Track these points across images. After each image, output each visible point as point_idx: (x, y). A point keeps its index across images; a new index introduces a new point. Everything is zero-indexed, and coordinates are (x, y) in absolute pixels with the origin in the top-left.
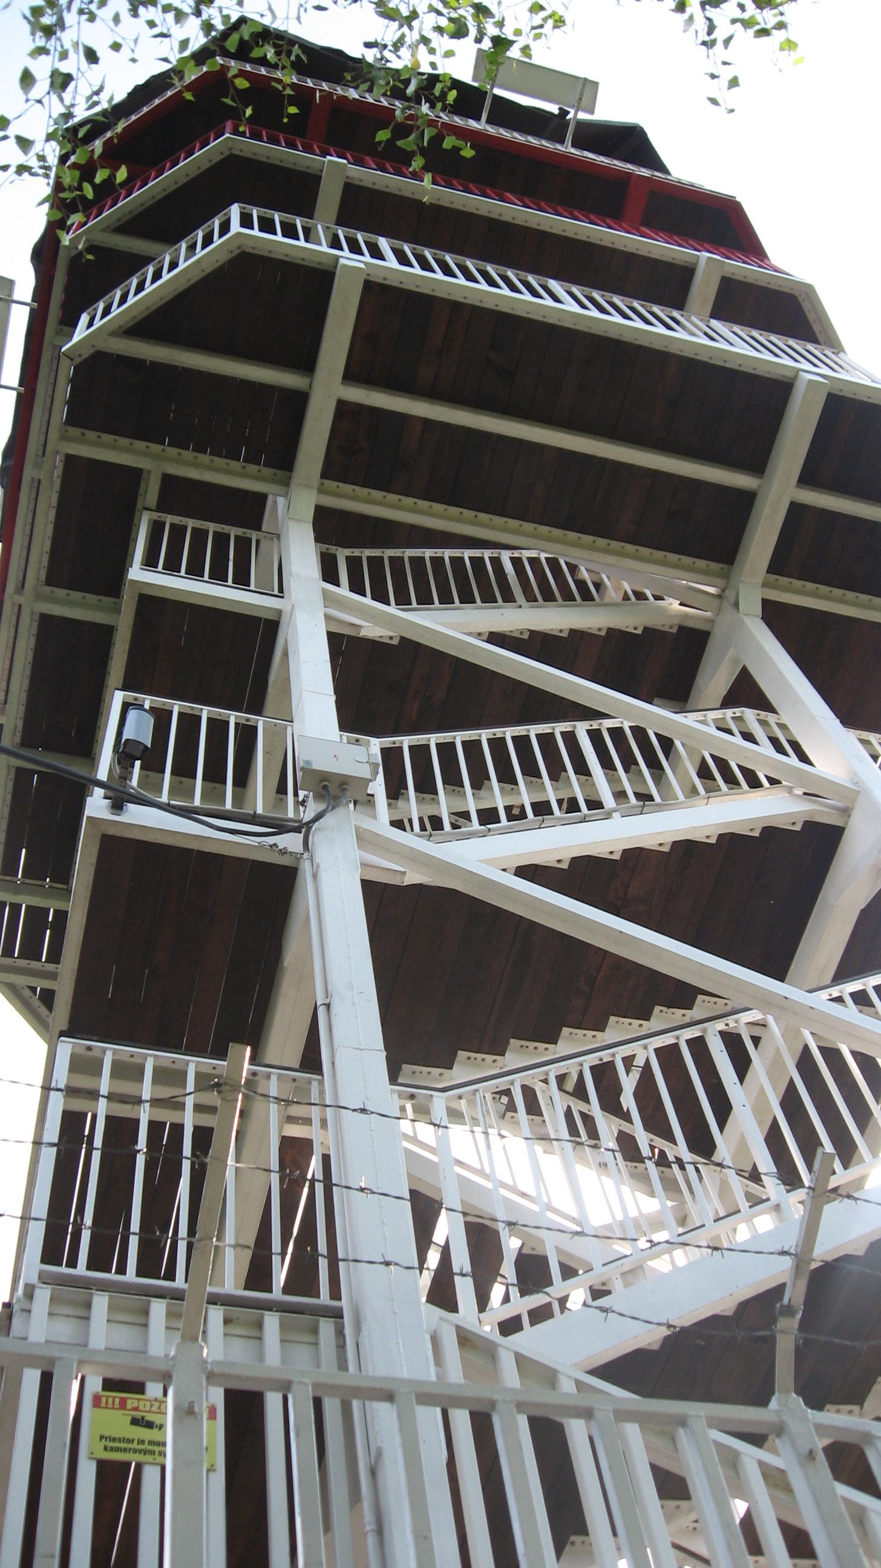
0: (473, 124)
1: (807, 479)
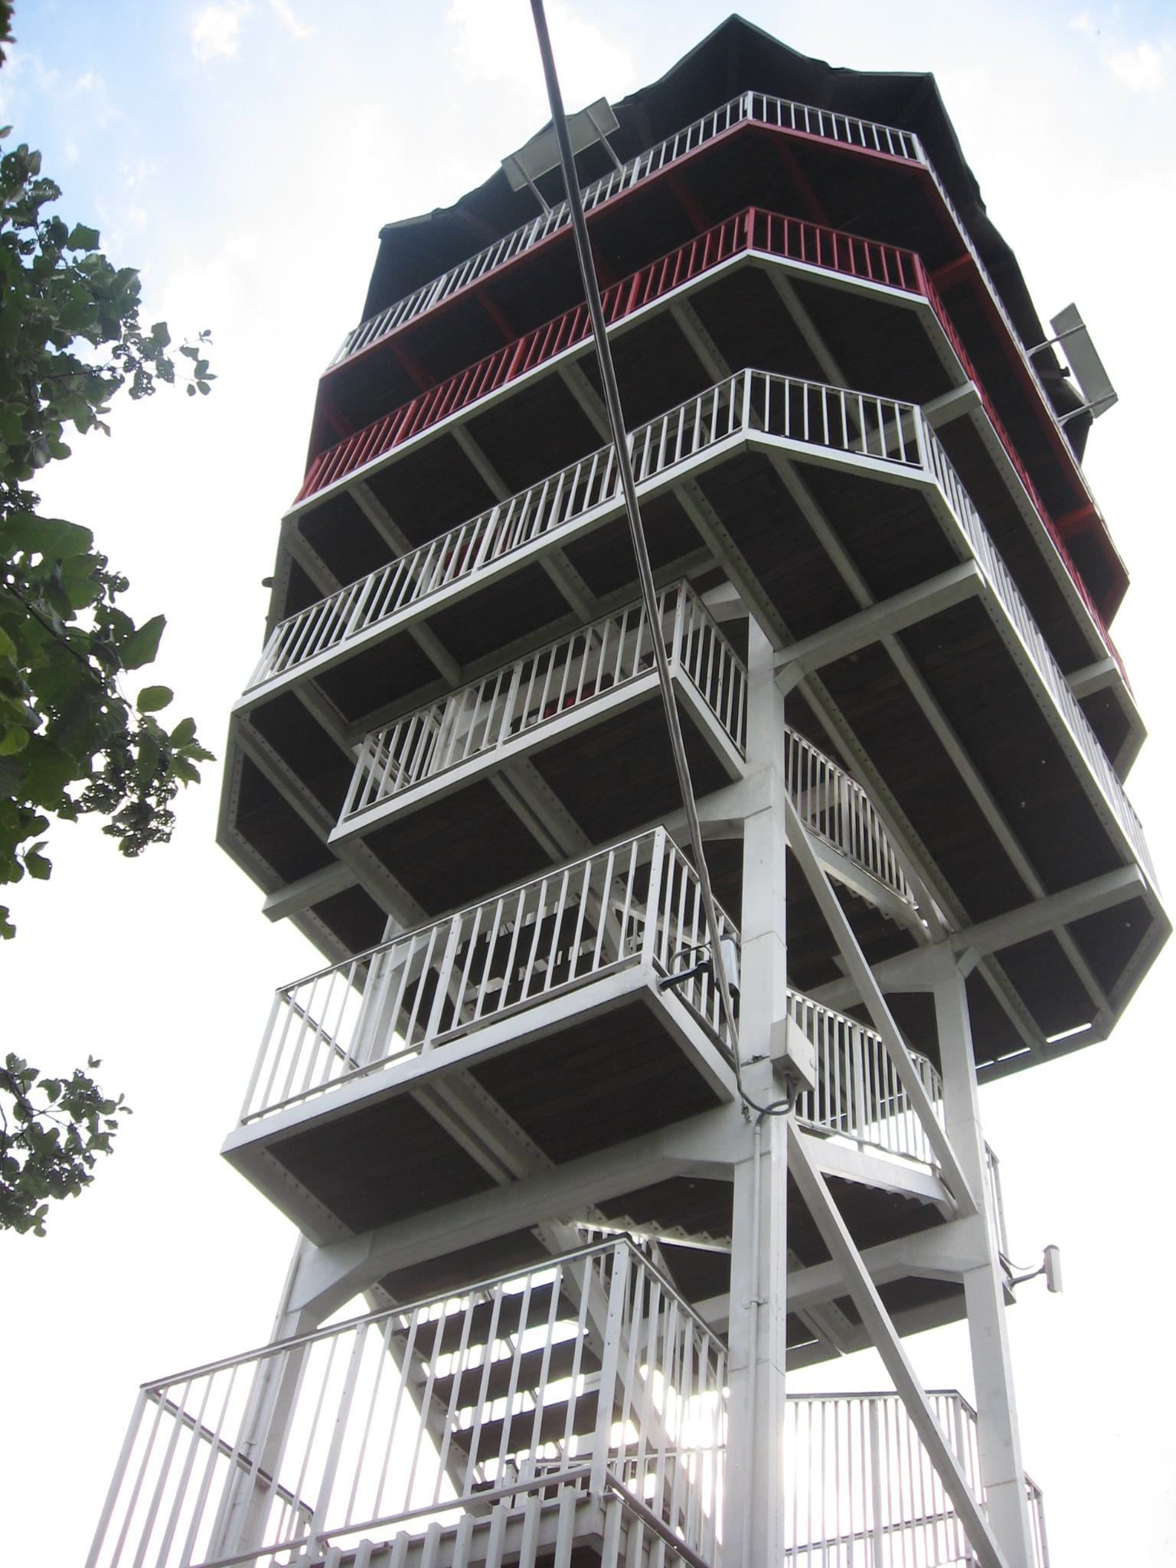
0: (1020, 347)
1: (905, 637)
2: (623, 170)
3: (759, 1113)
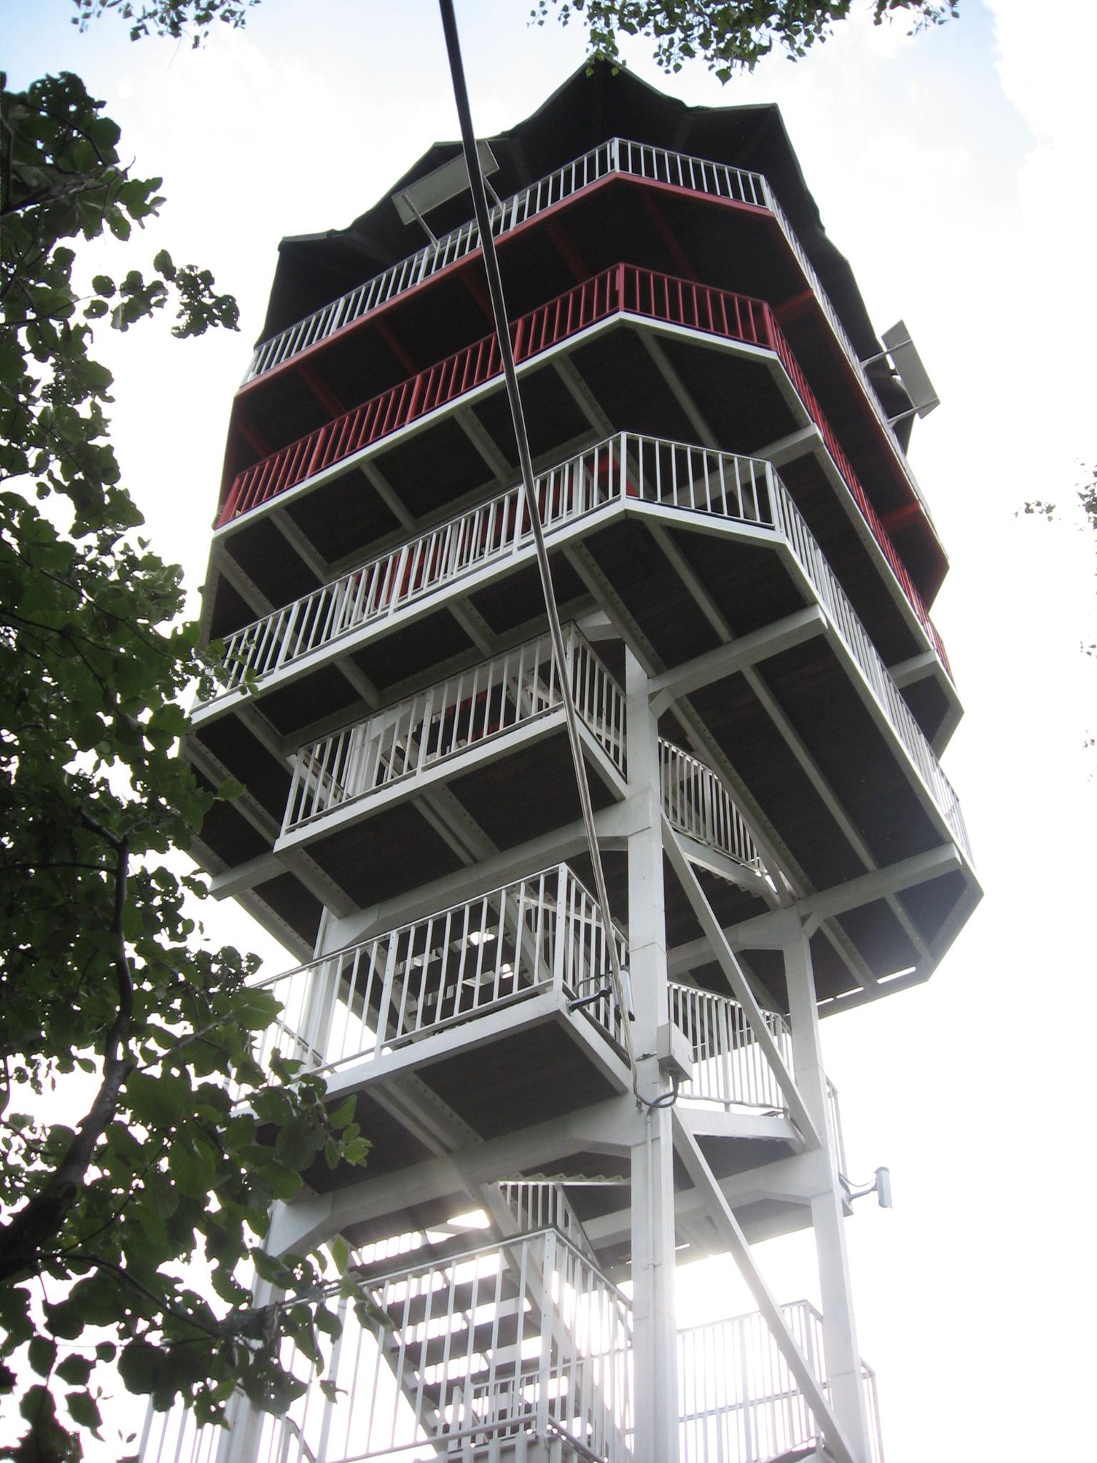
2: (502, 207)
3: (648, 1107)
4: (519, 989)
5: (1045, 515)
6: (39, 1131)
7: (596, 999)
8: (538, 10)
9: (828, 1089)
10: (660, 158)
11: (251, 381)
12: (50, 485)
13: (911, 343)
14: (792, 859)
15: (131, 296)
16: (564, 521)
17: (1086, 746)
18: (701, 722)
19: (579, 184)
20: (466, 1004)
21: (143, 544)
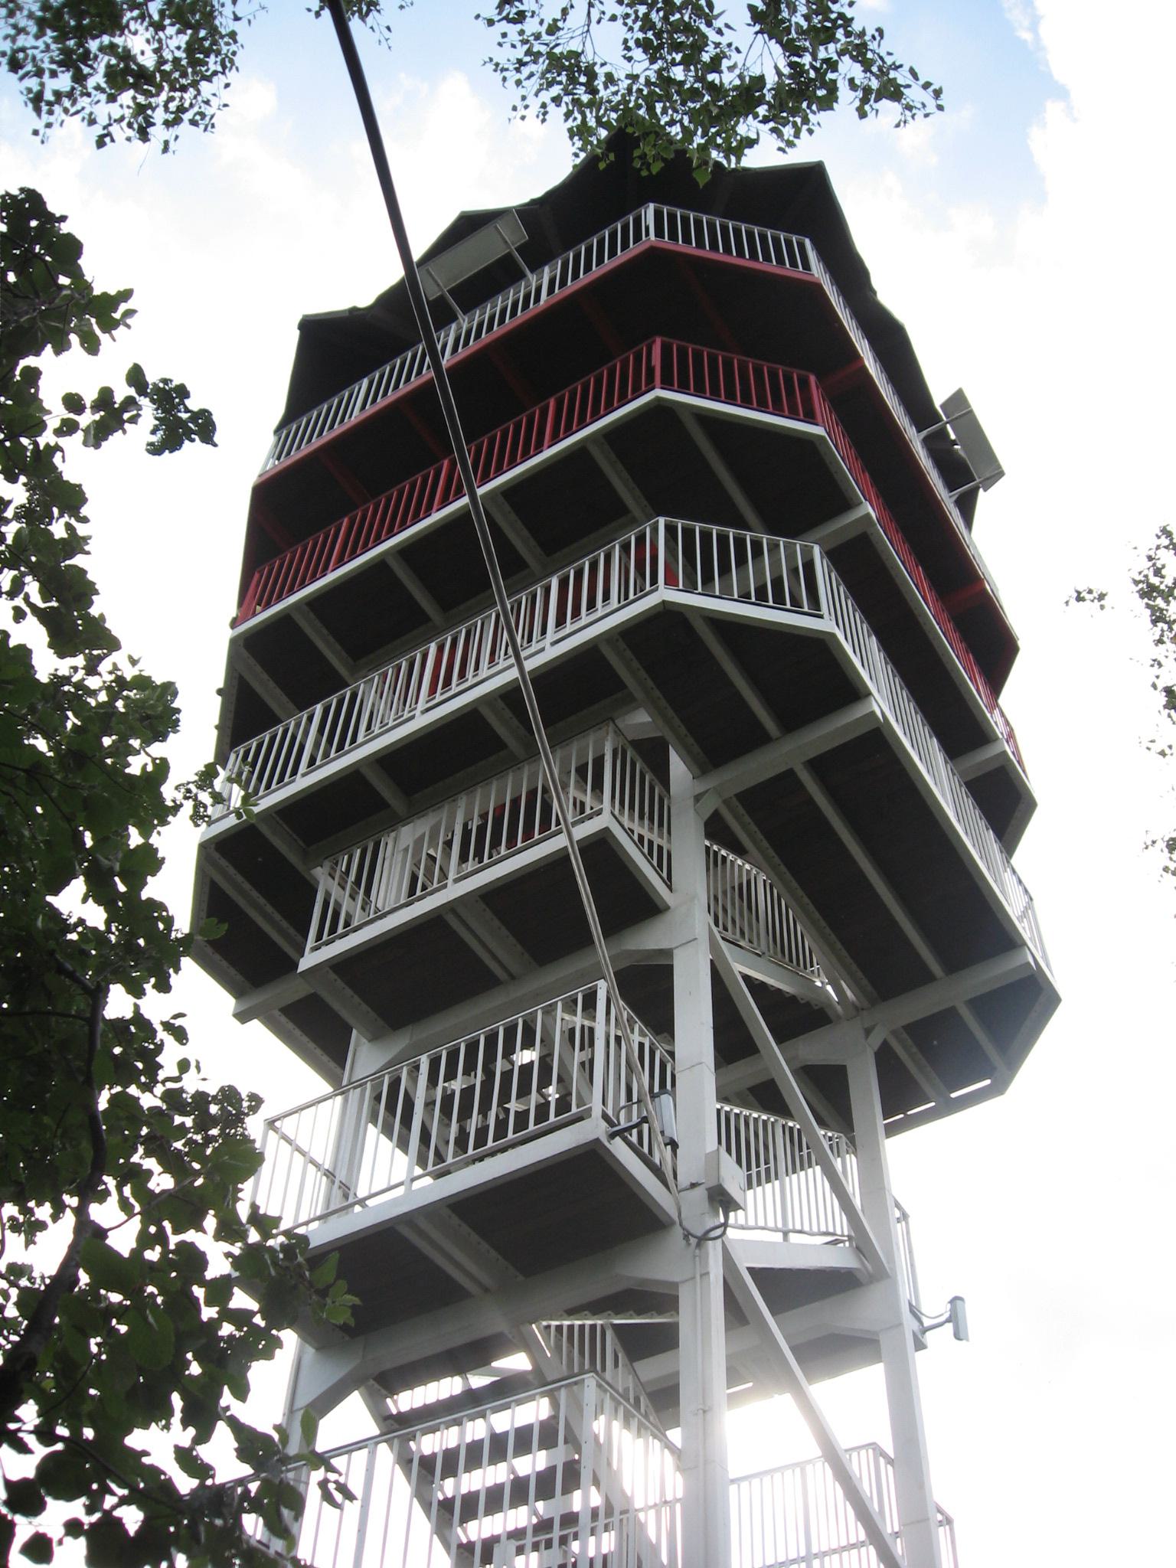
2: (533, 279)
4: (556, 1116)
5: (1097, 604)
6: (38, 1281)
7: (637, 1125)
8: (519, 104)
9: (897, 1214)
10: (698, 223)
11: (271, 469)
12: (27, 610)
13: (971, 412)
14: (854, 967)
15: (102, 413)
16: (599, 614)
17: (1147, 848)
18: (752, 823)
19: (613, 253)
20: (481, 1140)
21: (134, 662)
